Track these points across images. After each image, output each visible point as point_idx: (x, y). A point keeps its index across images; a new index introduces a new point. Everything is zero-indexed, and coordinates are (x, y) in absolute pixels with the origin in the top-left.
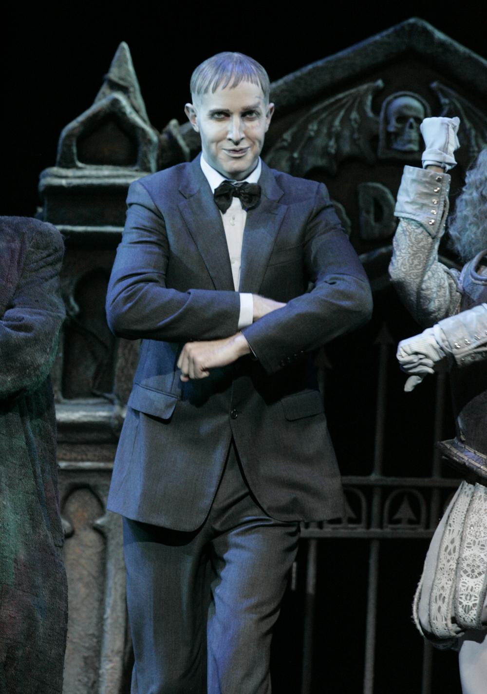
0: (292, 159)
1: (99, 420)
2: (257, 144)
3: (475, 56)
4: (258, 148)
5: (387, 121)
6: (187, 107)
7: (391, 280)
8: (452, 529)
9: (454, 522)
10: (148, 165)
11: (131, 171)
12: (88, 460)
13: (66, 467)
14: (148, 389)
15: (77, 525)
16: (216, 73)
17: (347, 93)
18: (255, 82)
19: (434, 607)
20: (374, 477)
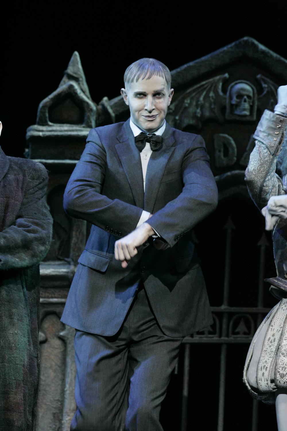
1: (62, 273)
2: (163, 113)
3: (283, 59)
4: (163, 115)
5: (231, 98)
6: (122, 90)
7: (124, 265)
8: (273, 328)
9: (274, 324)
10: (90, 124)
11: (81, 127)
12: (55, 298)
13: (43, 301)
14: (92, 253)
15: (49, 336)
16: (139, 70)
17: (207, 81)
18: (161, 76)
19: (260, 373)
20: (224, 307)
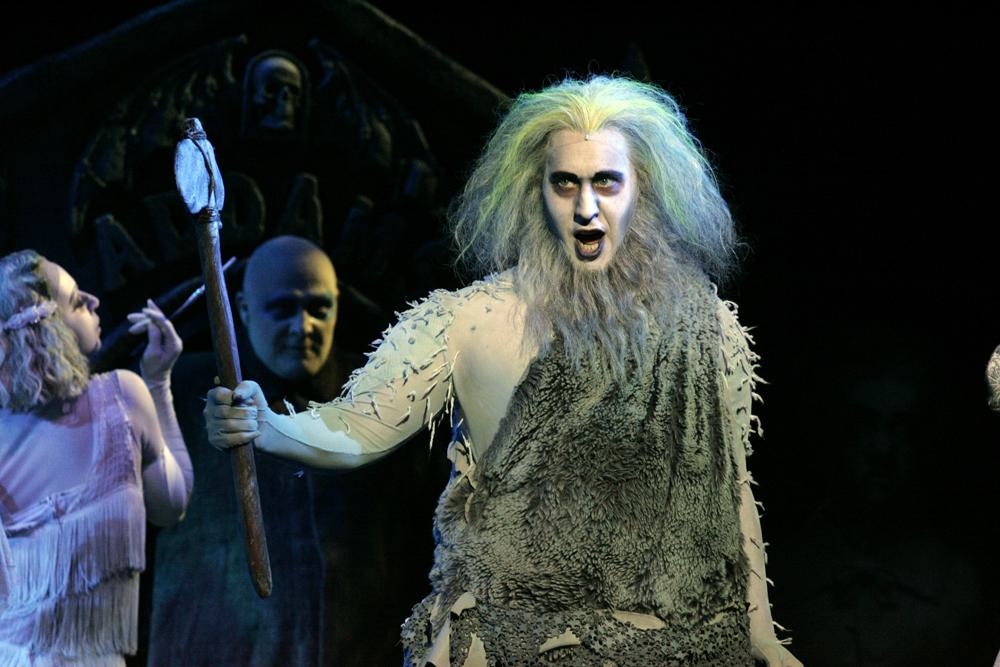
0: (127, 137)
5: (252, 90)
